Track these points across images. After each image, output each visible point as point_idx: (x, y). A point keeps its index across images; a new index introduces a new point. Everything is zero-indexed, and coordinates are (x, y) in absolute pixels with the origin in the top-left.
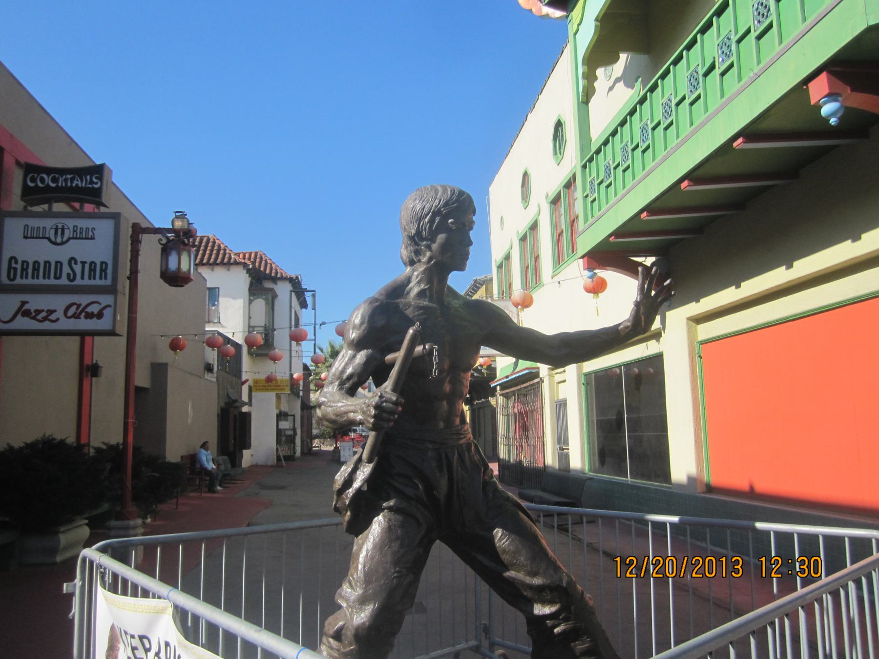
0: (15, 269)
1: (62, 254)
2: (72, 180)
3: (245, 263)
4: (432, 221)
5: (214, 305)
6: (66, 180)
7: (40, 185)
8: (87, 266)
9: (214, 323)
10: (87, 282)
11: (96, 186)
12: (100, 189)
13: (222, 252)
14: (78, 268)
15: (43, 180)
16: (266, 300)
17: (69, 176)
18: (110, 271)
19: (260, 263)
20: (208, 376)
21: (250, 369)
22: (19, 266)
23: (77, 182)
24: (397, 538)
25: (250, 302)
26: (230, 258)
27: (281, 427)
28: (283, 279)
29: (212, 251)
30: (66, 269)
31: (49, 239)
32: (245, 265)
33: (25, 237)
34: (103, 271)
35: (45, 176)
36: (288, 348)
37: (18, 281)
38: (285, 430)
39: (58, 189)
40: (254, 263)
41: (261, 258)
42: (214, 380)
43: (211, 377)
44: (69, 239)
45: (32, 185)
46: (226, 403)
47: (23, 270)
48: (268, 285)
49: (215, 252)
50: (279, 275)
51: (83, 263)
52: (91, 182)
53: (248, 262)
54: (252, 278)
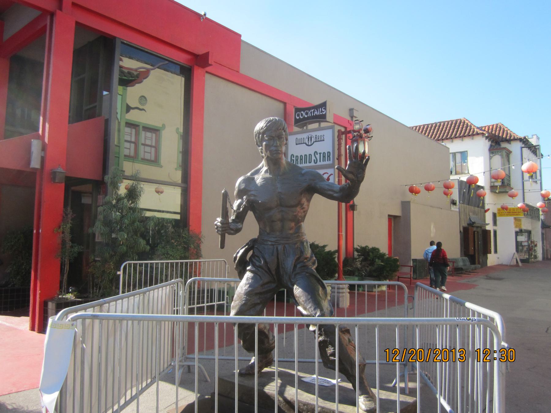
0: (293, 160)
1: (309, 151)
2: (314, 111)
3: (483, 133)
4: (259, 137)
5: (465, 162)
6: (311, 113)
7: (301, 117)
8: (322, 155)
9: (465, 174)
10: (322, 163)
11: (324, 113)
12: (326, 114)
13: (469, 128)
14: (318, 156)
15: (302, 115)
16: (502, 156)
17: (312, 110)
18: (331, 156)
19: (500, 131)
20: (454, 208)
21: (491, 202)
22: (295, 159)
23: (316, 113)
24: (248, 284)
25: (491, 158)
26: (474, 131)
27: (518, 240)
28: (515, 139)
29: (462, 128)
30: (313, 158)
31: (306, 143)
32: (483, 134)
33: (297, 144)
34: (329, 156)
35: (303, 112)
36: (521, 188)
37: (319, 163)
38: (522, 242)
39: (308, 118)
40: (488, 132)
41: (500, 127)
42: (458, 210)
43: (455, 209)
44: (314, 142)
45: (298, 118)
46: (468, 224)
47: (296, 160)
48: (504, 145)
49: (464, 128)
50: (512, 138)
51: (320, 154)
52: (322, 111)
53: (485, 132)
54: (492, 142)
